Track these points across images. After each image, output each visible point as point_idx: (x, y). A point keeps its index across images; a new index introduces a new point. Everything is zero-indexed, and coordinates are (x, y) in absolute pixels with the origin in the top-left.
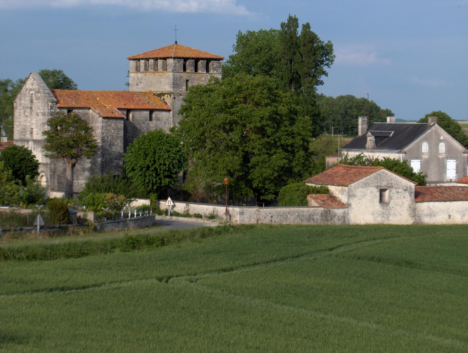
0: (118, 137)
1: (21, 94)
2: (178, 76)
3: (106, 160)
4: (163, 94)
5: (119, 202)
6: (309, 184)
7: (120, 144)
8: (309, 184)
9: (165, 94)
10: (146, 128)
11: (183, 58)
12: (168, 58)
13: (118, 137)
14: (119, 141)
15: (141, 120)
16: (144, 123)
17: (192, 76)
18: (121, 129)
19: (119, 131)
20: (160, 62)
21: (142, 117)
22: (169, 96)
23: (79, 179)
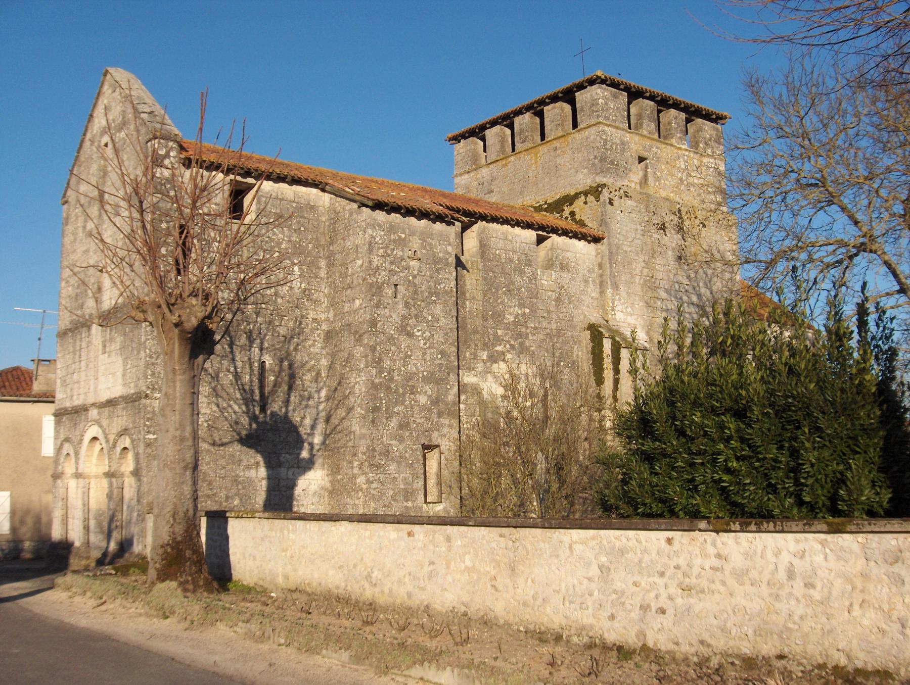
0: (437, 294)
1: (80, 166)
2: (617, 141)
3: (391, 379)
4: (570, 200)
5: (68, 300)
6: (203, 538)
7: (443, 321)
8: (203, 538)
9: (577, 196)
10: (529, 290)
11: (627, 89)
12: (581, 87)
13: (437, 294)
14: (439, 307)
15: (511, 261)
16: (522, 273)
17: (654, 149)
18: (447, 264)
19: (438, 271)
20: (553, 112)
21: (514, 252)
22: (591, 198)
23: (280, 465)
